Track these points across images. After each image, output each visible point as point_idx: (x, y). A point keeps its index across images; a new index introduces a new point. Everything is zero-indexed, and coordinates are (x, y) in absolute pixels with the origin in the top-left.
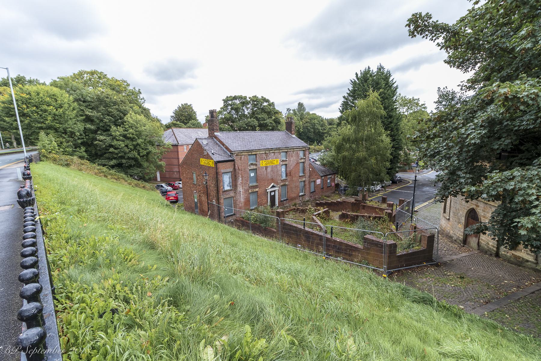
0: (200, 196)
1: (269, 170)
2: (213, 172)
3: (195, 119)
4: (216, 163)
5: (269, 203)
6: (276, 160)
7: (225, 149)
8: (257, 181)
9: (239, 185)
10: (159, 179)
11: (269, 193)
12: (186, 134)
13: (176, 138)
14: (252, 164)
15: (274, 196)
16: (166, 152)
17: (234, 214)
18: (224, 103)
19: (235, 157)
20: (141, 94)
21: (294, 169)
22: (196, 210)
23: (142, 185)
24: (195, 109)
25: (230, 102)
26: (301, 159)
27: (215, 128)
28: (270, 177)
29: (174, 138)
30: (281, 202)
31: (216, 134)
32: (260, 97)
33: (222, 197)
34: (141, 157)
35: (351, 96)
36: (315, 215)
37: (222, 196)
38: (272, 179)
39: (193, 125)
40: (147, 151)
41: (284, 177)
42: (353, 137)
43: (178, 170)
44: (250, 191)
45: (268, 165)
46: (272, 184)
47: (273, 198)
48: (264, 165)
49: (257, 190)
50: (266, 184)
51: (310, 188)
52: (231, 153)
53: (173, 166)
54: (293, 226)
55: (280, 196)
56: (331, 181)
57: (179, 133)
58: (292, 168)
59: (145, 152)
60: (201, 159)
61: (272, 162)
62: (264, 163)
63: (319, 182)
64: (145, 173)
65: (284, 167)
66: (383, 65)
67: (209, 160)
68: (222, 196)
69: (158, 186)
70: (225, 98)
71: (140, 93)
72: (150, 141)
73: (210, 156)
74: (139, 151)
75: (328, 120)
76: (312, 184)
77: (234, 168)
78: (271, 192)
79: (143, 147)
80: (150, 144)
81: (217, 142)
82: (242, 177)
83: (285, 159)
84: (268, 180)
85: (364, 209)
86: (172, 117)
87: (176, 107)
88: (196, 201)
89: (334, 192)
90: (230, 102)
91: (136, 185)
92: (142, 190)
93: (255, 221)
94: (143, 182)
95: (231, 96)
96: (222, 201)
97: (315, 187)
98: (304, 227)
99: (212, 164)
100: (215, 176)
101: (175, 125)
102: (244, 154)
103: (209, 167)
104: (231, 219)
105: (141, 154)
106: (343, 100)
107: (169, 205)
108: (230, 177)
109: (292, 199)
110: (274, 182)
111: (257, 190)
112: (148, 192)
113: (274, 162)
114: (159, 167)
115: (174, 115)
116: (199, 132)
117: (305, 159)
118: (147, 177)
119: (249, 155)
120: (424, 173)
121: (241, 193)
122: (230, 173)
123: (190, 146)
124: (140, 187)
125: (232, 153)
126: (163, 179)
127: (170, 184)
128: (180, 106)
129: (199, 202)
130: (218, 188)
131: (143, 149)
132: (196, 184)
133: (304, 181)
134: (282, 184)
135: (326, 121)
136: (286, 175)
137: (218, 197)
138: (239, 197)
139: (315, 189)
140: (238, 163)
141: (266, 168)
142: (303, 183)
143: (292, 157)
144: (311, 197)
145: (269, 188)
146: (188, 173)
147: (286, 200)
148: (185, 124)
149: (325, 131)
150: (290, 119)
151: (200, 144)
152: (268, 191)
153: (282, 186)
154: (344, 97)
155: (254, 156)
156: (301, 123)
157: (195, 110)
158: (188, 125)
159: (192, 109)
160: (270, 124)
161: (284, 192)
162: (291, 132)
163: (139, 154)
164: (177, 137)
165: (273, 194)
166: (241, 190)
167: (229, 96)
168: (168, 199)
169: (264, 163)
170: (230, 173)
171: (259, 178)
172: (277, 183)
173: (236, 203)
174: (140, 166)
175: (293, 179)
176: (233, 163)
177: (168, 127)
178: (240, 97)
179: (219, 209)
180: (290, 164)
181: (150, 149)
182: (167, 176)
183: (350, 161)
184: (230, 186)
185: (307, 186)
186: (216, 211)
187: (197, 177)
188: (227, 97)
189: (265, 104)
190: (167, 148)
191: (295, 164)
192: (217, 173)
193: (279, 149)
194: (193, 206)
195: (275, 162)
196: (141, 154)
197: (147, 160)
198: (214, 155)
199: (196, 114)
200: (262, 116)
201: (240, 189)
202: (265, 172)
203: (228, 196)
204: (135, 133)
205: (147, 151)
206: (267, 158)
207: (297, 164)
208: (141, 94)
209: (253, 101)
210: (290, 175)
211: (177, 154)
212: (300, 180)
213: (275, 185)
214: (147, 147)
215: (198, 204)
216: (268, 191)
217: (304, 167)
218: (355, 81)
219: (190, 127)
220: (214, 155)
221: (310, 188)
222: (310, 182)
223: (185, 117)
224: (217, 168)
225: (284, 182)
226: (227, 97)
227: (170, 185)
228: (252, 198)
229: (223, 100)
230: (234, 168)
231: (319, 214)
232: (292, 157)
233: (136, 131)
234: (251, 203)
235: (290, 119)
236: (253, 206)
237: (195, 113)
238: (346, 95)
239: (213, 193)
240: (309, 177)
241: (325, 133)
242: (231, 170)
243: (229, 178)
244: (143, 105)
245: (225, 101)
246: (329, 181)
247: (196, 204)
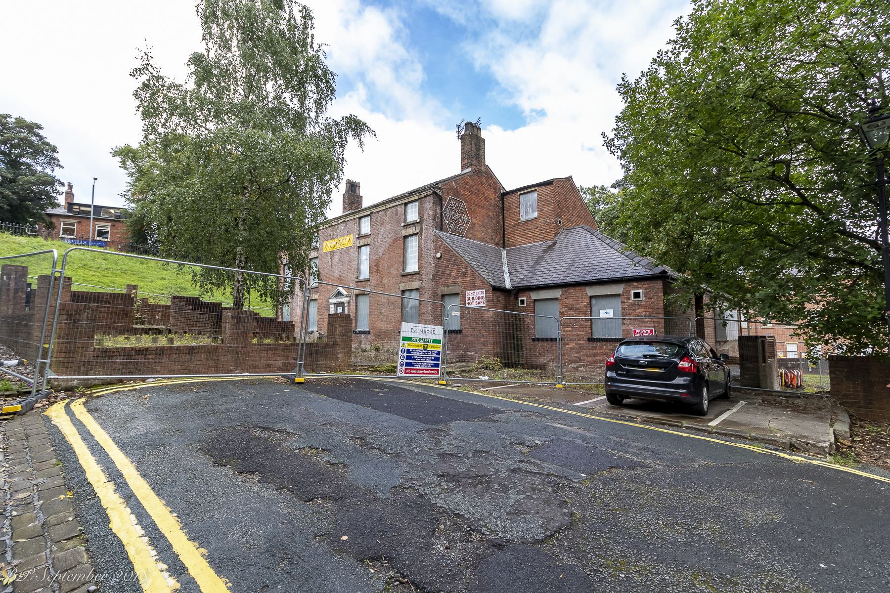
1: (336, 257)
48: (329, 249)
175: (385, 281)
191: (389, 241)
202: (330, 262)
232: (382, 224)
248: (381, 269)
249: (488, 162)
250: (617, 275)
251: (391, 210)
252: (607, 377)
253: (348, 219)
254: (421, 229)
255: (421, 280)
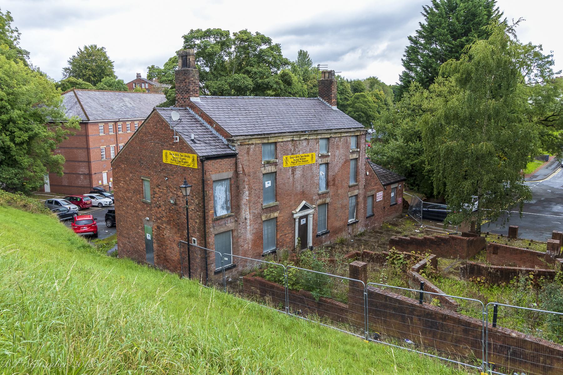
0: (158, 227)
1: (298, 173)
2: (194, 180)
3: (111, 74)
4: (202, 161)
5: (296, 241)
6: (310, 154)
7: (214, 132)
8: (276, 196)
9: (243, 206)
10: (47, 189)
11: (297, 220)
12: (102, 101)
13: (83, 108)
14: (268, 163)
15: (306, 225)
16: (69, 135)
17: (234, 266)
18: (185, 42)
19: (237, 147)
20: (12, 20)
21: (340, 173)
22: (148, 256)
23: (23, 203)
24: (111, 55)
25: (198, 42)
26: (353, 152)
27: (191, 88)
28: (299, 188)
29: (80, 109)
30: (317, 237)
31: (193, 99)
32: (254, 33)
33: (212, 231)
34: (16, 144)
35: (424, 37)
36: (418, 270)
37: (212, 229)
38: (303, 192)
39: (110, 86)
40: (30, 133)
41: (323, 189)
42: (465, 112)
43: (86, 171)
44: (264, 218)
45: (296, 165)
46: (304, 203)
47: (303, 229)
48: (289, 165)
49: (276, 214)
50: (292, 203)
51: (365, 208)
52: (228, 140)
53: (77, 164)
54: (391, 299)
55: (315, 225)
56: (396, 195)
57: (89, 100)
58: (337, 169)
59: (26, 135)
60: (164, 152)
61: (303, 159)
62: (290, 160)
63: (380, 196)
64: (25, 178)
65: (323, 168)
66: (235, 32)
67: (184, 154)
68: (212, 229)
69: (49, 202)
70: (186, 32)
71: (11, 19)
72: (35, 114)
73: (187, 146)
74: (12, 132)
75: (351, 82)
76: (370, 200)
77: (236, 172)
78: (301, 218)
79: (21, 126)
80: (35, 120)
81: (197, 116)
82: (250, 189)
83: (325, 153)
84: (296, 194)
85: (497, 254)
86: (66, 69)
87: (74, 52)
88: (149, 237)
89: (402, 217)
90: (198, 42)
91: (10, 203)
92: (21, 212)
93: (293, 285)
94: (23, 196)
95: (198, 31)
96: (211, 240)
97: (373, 207)
98: (421, 303)
99: (191, 161)
100: (200, 187)
101: (74, 84)
102: (254, 141)
103: (185, 169)
104: (228, 276)
105: (17, 140)
106: (409, 43)
107: (89, 246)
108: (228, 189)
109: (337, 231)
110: (306, 199)
111: (276, 214)
112: (34, 216)
113: (307, 158)
114: (52, 166)
115: (70, 67)
116: (126, 99)
117: (359, 152)
118: (29, 186)
119: (264, 144)
120: (538, 178)
121: (248, 221)
122: (228, 182)
123: (137, 124)
124: (17, 207)
125: (230, 139)
126: (57, 188)
127: (72, 198)
128: (83, 50)
129: (158, 240)
130: (204, 212)
131: (20, 129)
132: (151, 204)
133: (356, 196)
134: (319, 202)
135: (349, 85)
136: (327, 185)
137: (205, 231)
138: (243, 231)
139: (373, 210)
140: (243, 159)
141: (294, 169)
142: (353, 200)
143: (338, 148)
144: (366, 226)
145: (298, 210)
146: (131, 180)
147: (326, 233)
148: (95, 85)
149: (348, 102)
150: (327, 75)
151: (163, 121)
152: (295, 216)
153: (319, 206)
154: (410, 38)
155: (273, 147)
156: (305, 87)
157: (111, 59)
158: (99, 85)
159: (105, 56)
160: (275, 86)
161: (323, 218)
162: (329, 100)
163: (12, 140)
164: (85, 107)
165: (303, 222)
166: (248, 217)
167: (195, 29)
168: (77, 229)
169: (290, 160)
170: (228, 182)
171: (279, 191)
172: (312, 199)
173: (237, 242)
174: (13, 163)
175: (339, 191)
176: (233, 160)
177: (64, 87)
178: (218, 33)
179: (206, 256)
180: (334, 163)
181: (36, 130)
182: (65, 182)
183: (459, 160)
184: (227, 209)
185: (361, 206)
186: (198, 260)
187: (152, 189)
188: (192, 31)
189: (264, 47)
190: (70, 129)
191: (342, 162)
192: (203, 182)
193: (315, 132)
194: (142, 247)
195: (309, 159)
196: (17, 140)
197: (29, 153)
198: (195, 143)
199: (112, 66)
200: (260, 69)
201: (246, 213)
202: (291, 178)
203: (222, 230)
204: (6, 98)
205: (30, 133)
206: (295, 150)
207: (345, 162)
208: (12, 20)
209: (242, 40)
210: (334, 185)
211: (85, 139)
212: (350, 194)
213: (308, 205)
214: (30, 126)
215: (155, 245)
216: (295, 216)
217: (356, 167)
218: (431, 10)
219: (102, 89)
220: (195, 143)
221: (365, 208)
222: (365, 198)
223: (92, 70)
224: (203, 171)
225: (323, 197)
226: (192, 31)
227: (72, 200)
228: (267, 230)
229: (185, 37)
230: (236, 172)
231: (424, 267)
232: (338, 148)
233: (8, 94)
234: (265, 241)
235: (327, 75)
236: (268, 247)
237: (110, 64)
238: (414, 34)
239: (195, 223)
240: (365, 188)
241: (349, 105)
242: (230, 174)
243: (226, 191)
244: (15, 43)
245: (187, 39)
246: (392, 195)
247: (149, 245)
248: (336, 182)
249: (388, 84)
250: (217, 161)
251: (343, 138)
252: (383, 185)
253: (311, 137)
254: (359, 156)
255: (359, 189)
